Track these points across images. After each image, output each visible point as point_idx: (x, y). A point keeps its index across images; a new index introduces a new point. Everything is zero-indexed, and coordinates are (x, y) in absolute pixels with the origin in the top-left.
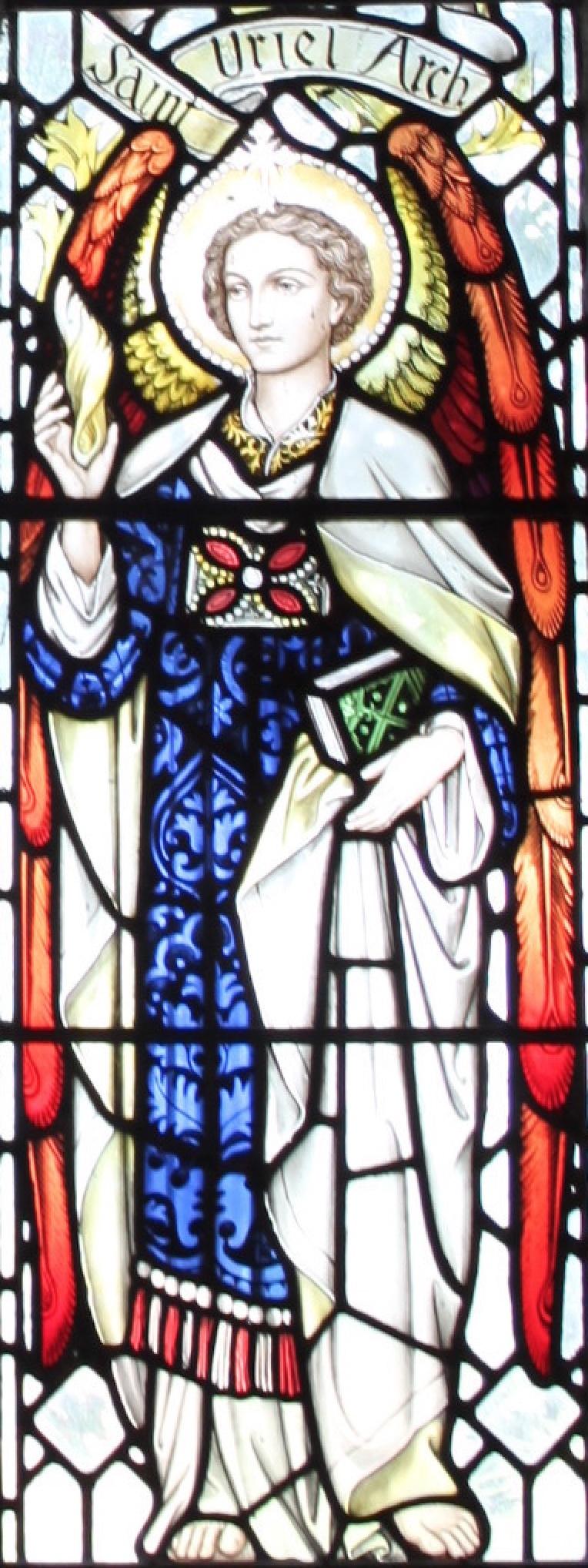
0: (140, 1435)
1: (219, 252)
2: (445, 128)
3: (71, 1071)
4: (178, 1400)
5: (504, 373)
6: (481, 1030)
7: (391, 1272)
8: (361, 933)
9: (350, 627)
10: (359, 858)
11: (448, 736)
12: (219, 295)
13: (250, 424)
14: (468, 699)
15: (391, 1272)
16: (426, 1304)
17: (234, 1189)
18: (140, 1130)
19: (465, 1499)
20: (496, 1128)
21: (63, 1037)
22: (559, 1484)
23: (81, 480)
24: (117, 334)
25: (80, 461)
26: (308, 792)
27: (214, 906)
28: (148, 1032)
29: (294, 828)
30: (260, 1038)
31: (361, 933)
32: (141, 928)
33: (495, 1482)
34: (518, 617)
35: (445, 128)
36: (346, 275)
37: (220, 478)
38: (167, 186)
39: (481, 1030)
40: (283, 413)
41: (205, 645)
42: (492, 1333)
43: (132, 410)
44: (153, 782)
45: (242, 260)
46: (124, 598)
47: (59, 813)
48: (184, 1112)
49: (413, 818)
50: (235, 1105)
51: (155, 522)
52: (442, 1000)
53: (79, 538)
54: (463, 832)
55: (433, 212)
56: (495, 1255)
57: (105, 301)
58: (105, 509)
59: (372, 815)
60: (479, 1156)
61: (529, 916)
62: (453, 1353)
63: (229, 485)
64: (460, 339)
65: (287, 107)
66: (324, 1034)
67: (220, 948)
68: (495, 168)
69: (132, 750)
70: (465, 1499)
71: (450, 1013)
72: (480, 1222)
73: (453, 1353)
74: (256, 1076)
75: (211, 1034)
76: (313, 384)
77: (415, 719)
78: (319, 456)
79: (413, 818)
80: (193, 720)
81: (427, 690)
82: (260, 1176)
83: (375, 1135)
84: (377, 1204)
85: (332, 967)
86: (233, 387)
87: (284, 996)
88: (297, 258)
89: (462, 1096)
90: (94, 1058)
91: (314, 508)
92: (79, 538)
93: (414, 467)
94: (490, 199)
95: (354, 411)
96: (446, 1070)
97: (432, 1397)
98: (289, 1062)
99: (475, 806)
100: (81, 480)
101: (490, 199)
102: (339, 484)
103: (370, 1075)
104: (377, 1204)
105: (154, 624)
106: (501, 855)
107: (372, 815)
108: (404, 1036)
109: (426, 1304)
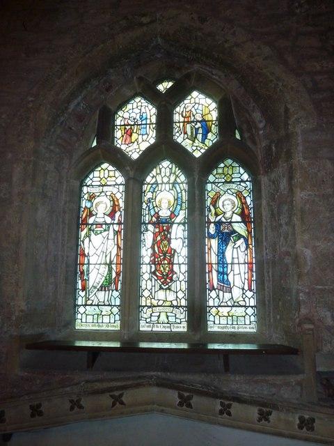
0: (218, 296)
1: (223, 202)
2: (103, 191)
3: (212, 267)
4: (221, 293)
5: (246, 211)
6: (245, 263)
7: (238, 282)
8: (235, 256)
9: (234, 232)
10: (235, 250)
11: (242, 240)
12: (223, 206)
13: (226, 216)
14: (243, 237)
15: (238, 282)
16: (241, 285)
17: (225, 276)
18: (218, 271)
19: (244, 301)
20: (246, 271)
21: (211, 264)
22: (252, 299)
23: (212, 221)
24: (215, 209)
25: (212, 219)
26: (230, 245)
27: (223, 253)
28: (218, 263)
29: (229, 248)
30: (227, 264)
31: (235, 256)
32: (217, 255)
33: (247, 299)
34: (248, 230)
35: (103, 191)
36: (233, 203)
37: (224, 220)
38: (219, 197)
39: (245, 263)
40: (228, 215)
41: (223, 233)
42: (246, 288)
43: (217, 215)
44: (219, 244)
45: (225, 203)
46: (216, 229)
47: (211, 247)
48: (221, 270)
49: (239, 246)
50: (225, 270)
51: (218, 224)
52: (242, 261)
53: (212, 225)
54: (243, 247)
55: (240, 199)
56: (246, 281)
57: (214, 206)
58: (214, 223)
59: (236, 246)
60: (245, 273)
61: (249, 254)
62: (243, 289)
63: (224, 221)
64: (243, 209)
65: (229, 191)
66: (232, 264)
67: (224, 257)
68: (245, 195)
69: (217, 241)
70: (244, 301)
71: (243, 262)
72: (163, 226)
73: (243, 289)
74: (227, 267)
75: (223, 263)
76: (231, 212)
77: (239, 239)
78: (231, 218)
79: (239, 246)
80: (222, 239)
81: (240, 236)
82: (227, 275)
83: (237, 271)
84: (237, 277)
85: (233, 258)
86: (224, 213)
87: (229, 261)
88: (230, 202)
89: (244, 268)
90: (214, 266)
91: (231, 222)
92: (212, 225)
93: (238, 218)
94: (245, 198)
95: (234, 215)
96: (242, 267)
97: (242, 293)
98: (229, 266)
99: (244, 245)
100: (212, 221)
101: (245, 198)
102: (233, 220)
103: (236, 267)
104: (237, 277)
105: (218, 231)
106: (246, 249)
107: (236, 246)
108: (239, 264)
109: (241, 285)
